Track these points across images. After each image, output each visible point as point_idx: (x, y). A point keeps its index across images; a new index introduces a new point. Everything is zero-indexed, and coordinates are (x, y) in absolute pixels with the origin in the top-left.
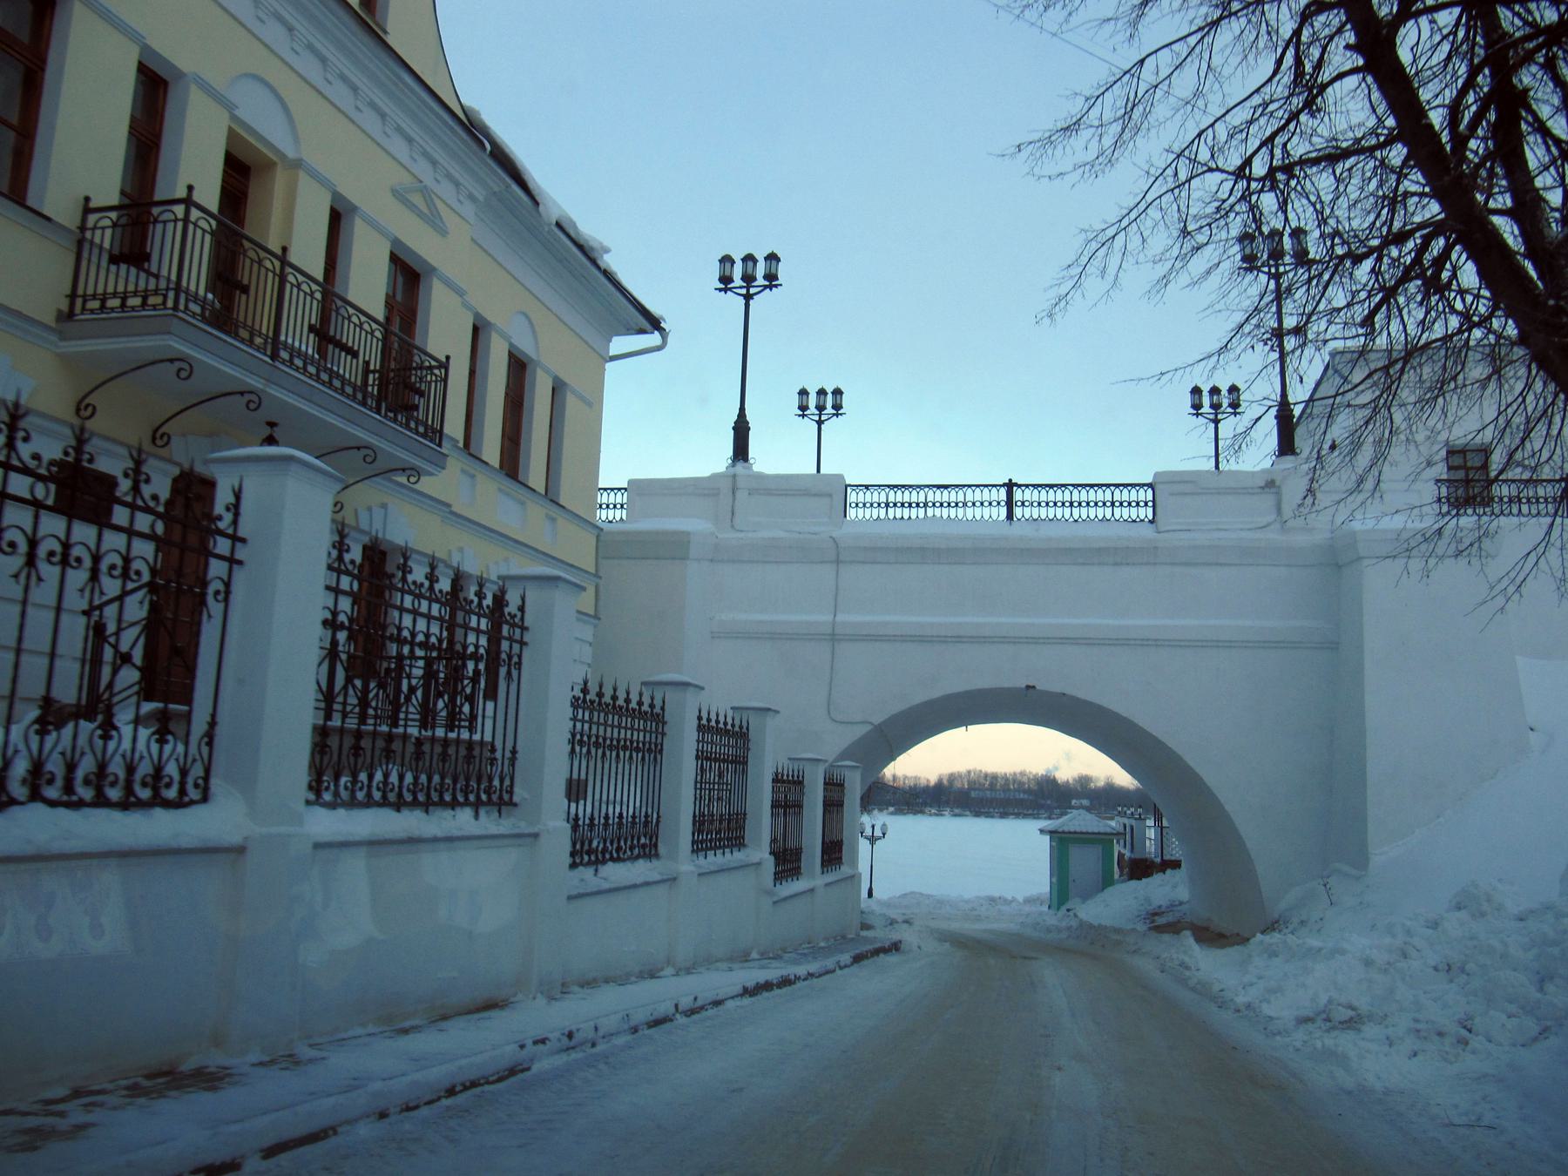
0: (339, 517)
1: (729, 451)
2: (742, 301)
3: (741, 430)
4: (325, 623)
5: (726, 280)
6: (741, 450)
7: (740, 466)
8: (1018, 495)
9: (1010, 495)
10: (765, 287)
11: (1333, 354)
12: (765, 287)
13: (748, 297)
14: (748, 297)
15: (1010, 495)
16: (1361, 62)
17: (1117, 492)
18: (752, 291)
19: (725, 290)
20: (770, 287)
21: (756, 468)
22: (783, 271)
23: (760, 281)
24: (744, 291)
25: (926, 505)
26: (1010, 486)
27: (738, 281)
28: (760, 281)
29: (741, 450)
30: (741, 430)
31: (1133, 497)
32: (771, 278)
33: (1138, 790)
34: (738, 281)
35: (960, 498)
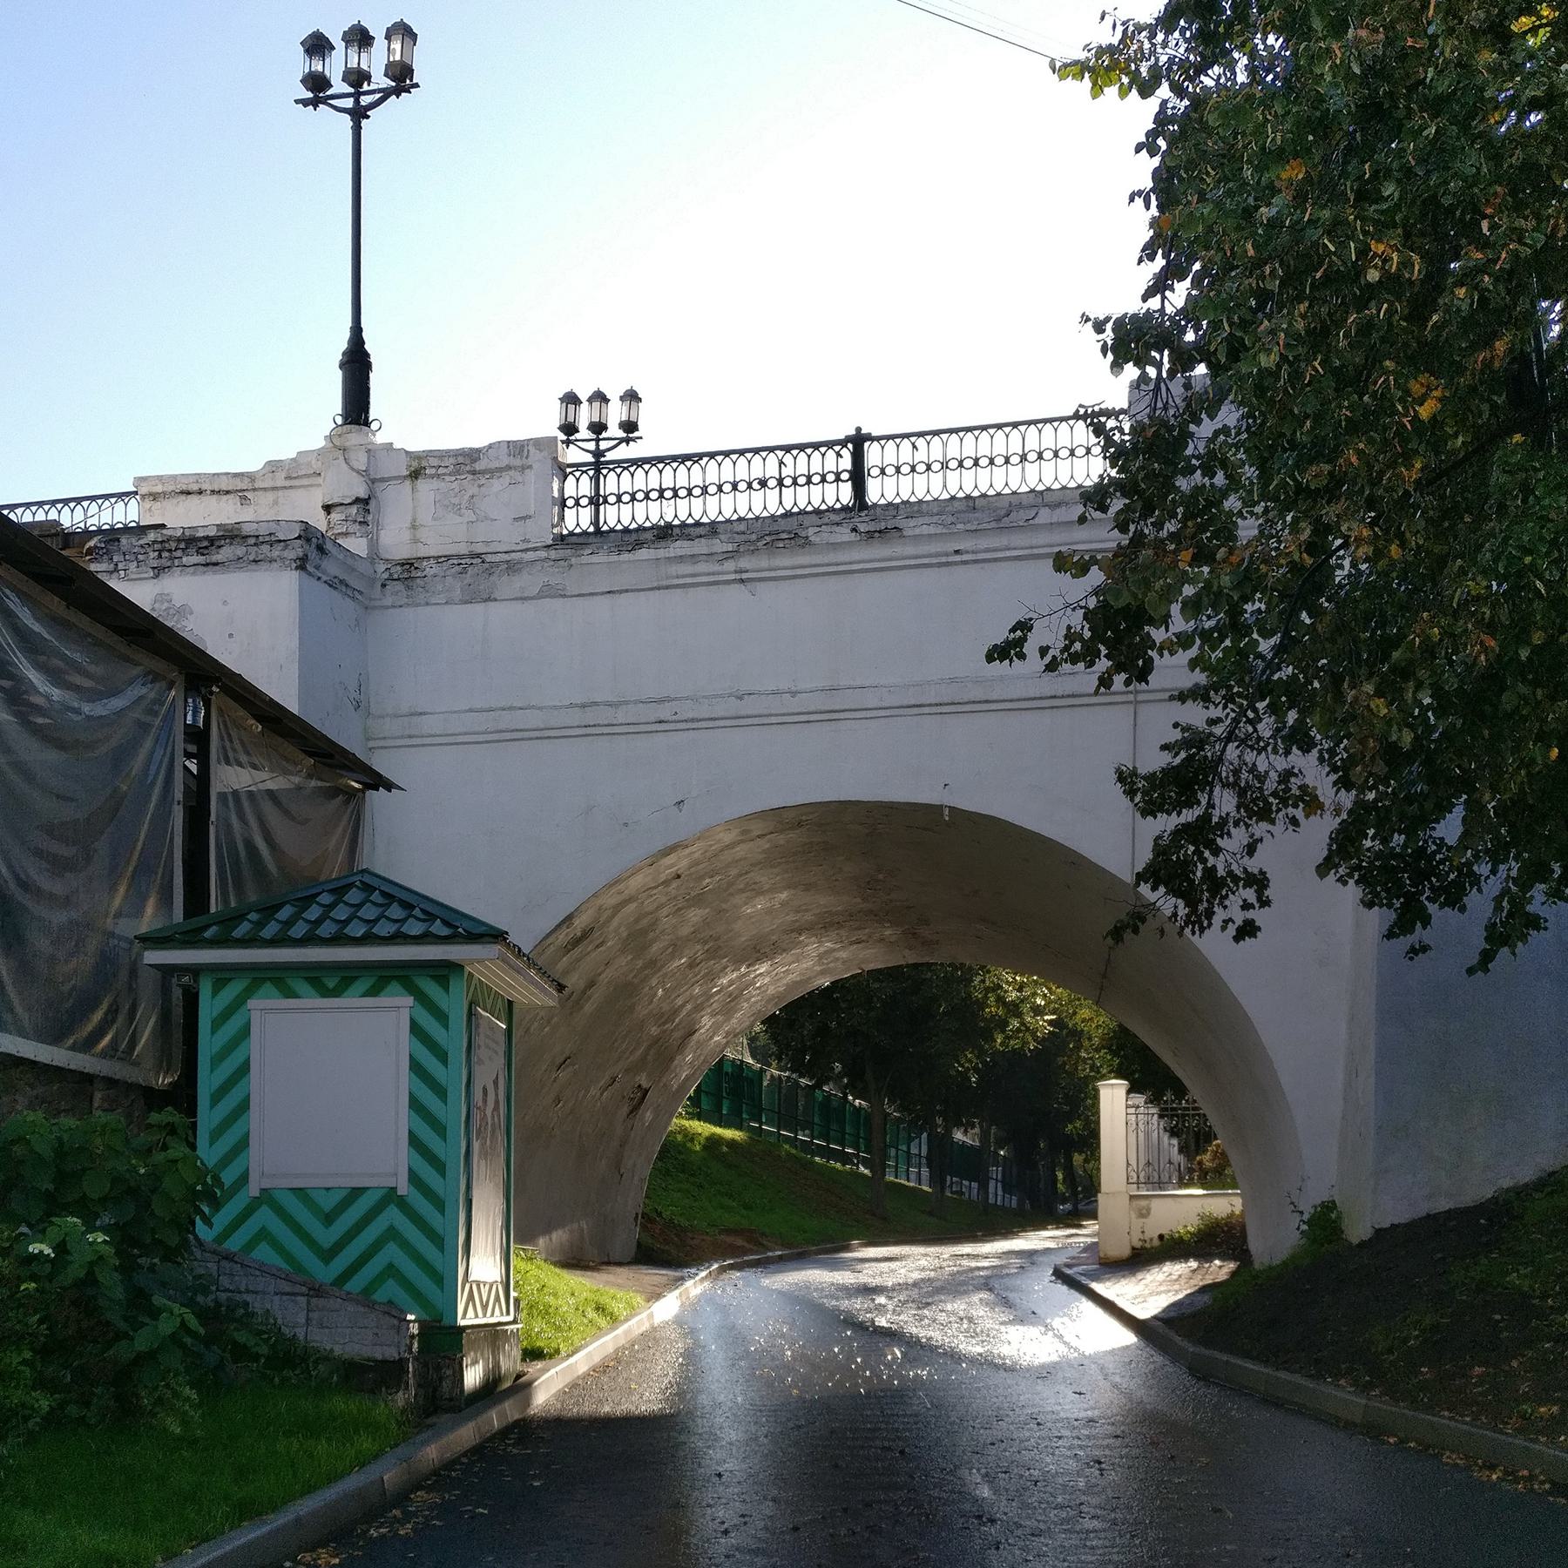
2: (347, 120)
3: (357, 364)
5: (317, 84)
6: (357, 407)
7: (355, 436)
8: (872, 454)
9: (858, 457)
10: (621, 441)
11: (1424, 202)
12: (621, 441)
13: (359, 114)
15: (858, 457)
16: (1506, 949)
18: (365, 100)
19: (315, 103)
20: (398, 91)
21: (380, 439)
24: (348, 103)
26: (858, 441)
27: (584, 433)
28: (380, 80)
29: (357, 407)
30: (357, 364)
32: (402, 78)
33: (1234, 1274)
34: (339, 86)
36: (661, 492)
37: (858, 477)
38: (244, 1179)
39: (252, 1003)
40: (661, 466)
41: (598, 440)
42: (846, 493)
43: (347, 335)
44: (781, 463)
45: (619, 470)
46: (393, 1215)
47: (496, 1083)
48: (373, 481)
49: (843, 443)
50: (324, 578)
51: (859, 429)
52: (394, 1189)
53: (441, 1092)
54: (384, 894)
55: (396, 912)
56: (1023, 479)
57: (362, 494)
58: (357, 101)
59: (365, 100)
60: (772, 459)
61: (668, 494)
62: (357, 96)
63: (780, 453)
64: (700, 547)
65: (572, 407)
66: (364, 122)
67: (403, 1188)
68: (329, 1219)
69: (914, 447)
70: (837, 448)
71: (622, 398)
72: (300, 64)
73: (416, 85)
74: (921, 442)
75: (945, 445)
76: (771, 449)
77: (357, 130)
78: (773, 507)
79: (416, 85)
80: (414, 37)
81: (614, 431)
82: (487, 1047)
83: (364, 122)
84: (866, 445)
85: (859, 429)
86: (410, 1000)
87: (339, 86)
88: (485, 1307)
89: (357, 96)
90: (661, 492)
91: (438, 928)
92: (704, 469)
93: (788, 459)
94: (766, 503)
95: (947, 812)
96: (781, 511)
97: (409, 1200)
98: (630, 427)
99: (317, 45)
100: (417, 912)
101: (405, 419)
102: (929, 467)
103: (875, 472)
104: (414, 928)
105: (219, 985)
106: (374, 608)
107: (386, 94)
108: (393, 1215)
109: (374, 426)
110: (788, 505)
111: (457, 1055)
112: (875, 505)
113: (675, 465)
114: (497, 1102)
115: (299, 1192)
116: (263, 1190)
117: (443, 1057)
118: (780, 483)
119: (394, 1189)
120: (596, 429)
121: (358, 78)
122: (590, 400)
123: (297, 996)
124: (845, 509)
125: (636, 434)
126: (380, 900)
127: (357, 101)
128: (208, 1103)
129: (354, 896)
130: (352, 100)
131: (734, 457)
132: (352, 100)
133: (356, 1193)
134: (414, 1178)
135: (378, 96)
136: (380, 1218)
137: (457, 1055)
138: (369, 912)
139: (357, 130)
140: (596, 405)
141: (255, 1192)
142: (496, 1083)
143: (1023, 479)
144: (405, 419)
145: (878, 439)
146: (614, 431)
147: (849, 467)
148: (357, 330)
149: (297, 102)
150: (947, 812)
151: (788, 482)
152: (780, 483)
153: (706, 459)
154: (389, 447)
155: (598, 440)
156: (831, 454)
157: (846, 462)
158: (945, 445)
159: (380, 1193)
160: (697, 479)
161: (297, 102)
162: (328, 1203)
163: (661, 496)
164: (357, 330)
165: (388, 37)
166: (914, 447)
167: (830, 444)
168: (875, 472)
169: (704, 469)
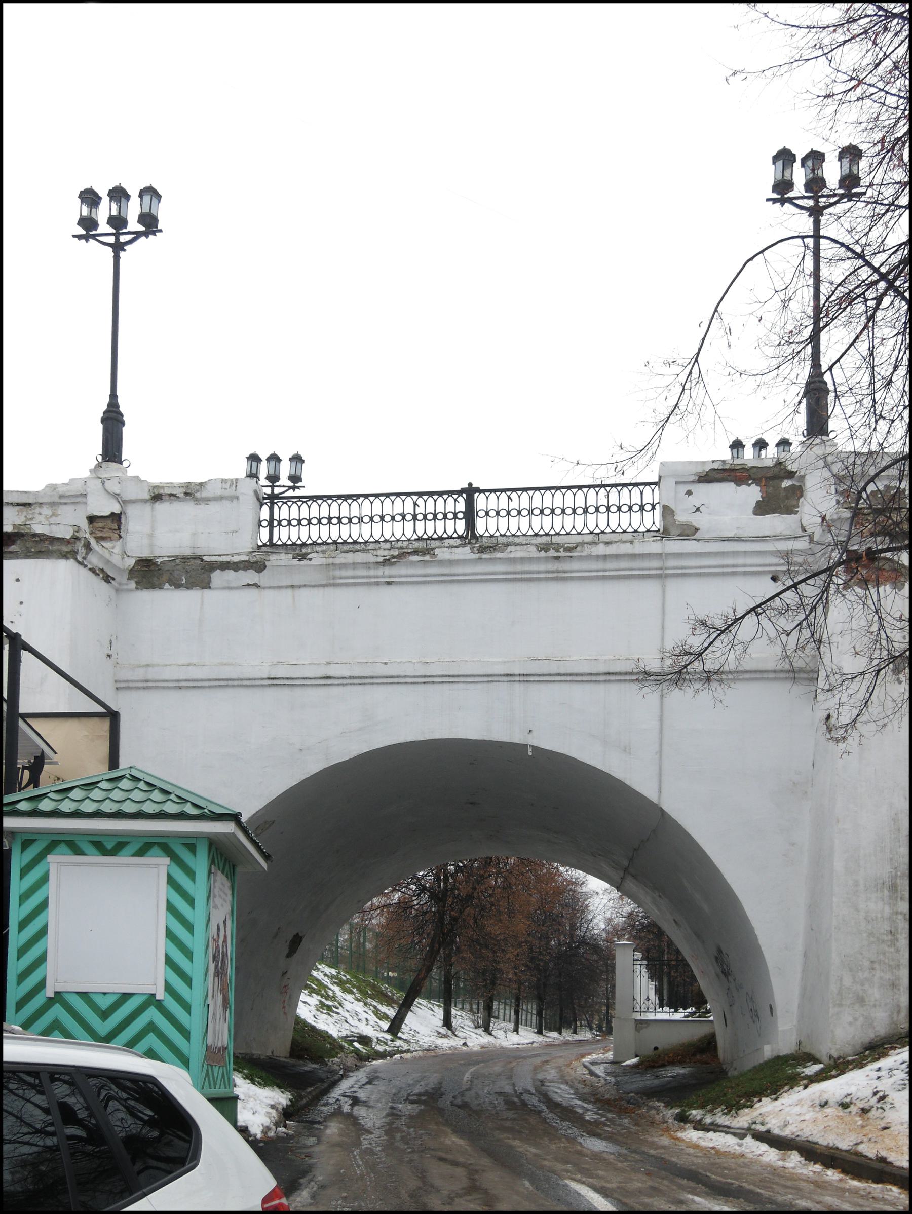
0: (182, 495)
1: (97, 448)
3: (113, 420)
4: (87, 241)
5: (88, 224)
6: (112, 449)
8: (480, 502)
9: (470, 503)
13: (118, 248)
14: (118, 248)
15: (470, 503)
17: (440, 501)
19: (86, 237)
20: (146, 234)
21: (131, 472)
22: (164, 213)
23: (134, 225)
25: (531, 512)
26: (470, 492)
28: (134, 225)
29: (112, 449)
30: (113, 420)
31: (314, 512)
32: (150, 223)
34: (104, 227)
35: (636, 499)
36: (330, 519)
37: (470, 516)
38: (42, 985)
39: (50, 858)
40: (330, 501)
41: (273, 487)
42: (461, 526)
43: (107, 400)
44: (415, 504)
45: (299, 503)
46: (152, 1014)
47: (225, 922)
48: (125, 502)
49: (460, 493)
50: (90, 566)
51: (470, 485)
52: (153, 995)
53: (189, 927)
54: (147, 783)
55: (156, 796)
56: (585, 524)
57: (117, 511)
58: (117, 239)
59: (123, 239)
60: (409, 501)
61: (335, 521)
62: (117, 235)
63: (415, 498)
64: (360, 557)
65: (254, 464)
66: (122, 254)
67: (161, 995)
68: (104, 1015)
69: (509, 497)
70: (455, 496)
71: (290, 459)
72: (76, 209)
73: (161, 231)
74: (514, 496)
75: (531, 498)
76: (409, 494)
77: (117, 259)
78: (409, 534)
79: (161, 231)
80: (159, 197)
81: (284, 481)
82: (220, 896)
83: (122, 254)
84: (476, 495)
85: (470, 485)
86: (167, 860)
87: (104, 227)
88: (215, 1084)
89: (117, 235)
90: (330, 519)
91: (190, 810)
92: (360, 506)
93: (420, 501)
94: (404, 531)
95: (530, 750)
96: (415, 537)
97: (164, 1003)
98: (295, 479)
99: (90, 197)
100: (172, 797)
101: (149, 459)
102: (519, 513)
103: (482, 514)
104: (171, 808)
105: (26, 844)
106: (122, 590)
107: (138, 235)
108: (152, 1014)
109: (125, 464)
110: (420, 532)
111: (200, 901)
112: (481, 536)
113: (340, 501)
114: (225, 936)
115: (84, 995)
116: (56, 993)
117: (191, 902)
118: (415, 517)
119: (153, 995)
120: (274, 481)
121: (118, 222)
122: (268, 459)
123: (83, 854)
124: (459, 537)
125: (299, 484)
126: (146, 788)
127: (117, 239)
128: (16, 928)
129: (125, 784)
130: (113, 238)
131: (382, 498)
132: (113, 238)
133: (125, 997)
134: (169, 988)
135: (133, 236)
136: (39, 1021)
137: (200, 901)
138: (137, 795)
139: (117, 259)
140: (272, 463)
141: (51, 994)
142: (225, 922)
143: (585, 524)
144: (149, 459)
145: (484, 491)
146: (284, 481)
147: (463, 510)
148: (113, 396)
149: (74, 236)
150: (530, 750)
151: (420, 517)
152: (415, 517)
153: (362, 499)
154: (137, 479)
155: (273, 487)
156: (450, 500)
157: (461, 506)
158: (531, 498)
159: (144, 998)
160: (355, 512)
161: (74, 236)
162: (104, 1003)
163: (330, 522)
164: (113, 396)
165: (141, 196)
166: (509, 497)
167: (450, 493)
168: (482, 514)
169: (360, 506)
